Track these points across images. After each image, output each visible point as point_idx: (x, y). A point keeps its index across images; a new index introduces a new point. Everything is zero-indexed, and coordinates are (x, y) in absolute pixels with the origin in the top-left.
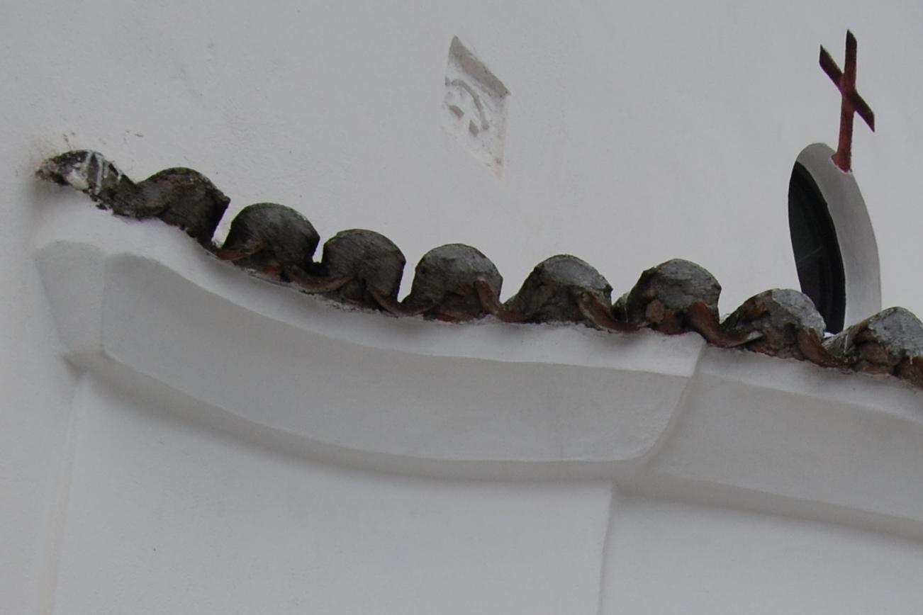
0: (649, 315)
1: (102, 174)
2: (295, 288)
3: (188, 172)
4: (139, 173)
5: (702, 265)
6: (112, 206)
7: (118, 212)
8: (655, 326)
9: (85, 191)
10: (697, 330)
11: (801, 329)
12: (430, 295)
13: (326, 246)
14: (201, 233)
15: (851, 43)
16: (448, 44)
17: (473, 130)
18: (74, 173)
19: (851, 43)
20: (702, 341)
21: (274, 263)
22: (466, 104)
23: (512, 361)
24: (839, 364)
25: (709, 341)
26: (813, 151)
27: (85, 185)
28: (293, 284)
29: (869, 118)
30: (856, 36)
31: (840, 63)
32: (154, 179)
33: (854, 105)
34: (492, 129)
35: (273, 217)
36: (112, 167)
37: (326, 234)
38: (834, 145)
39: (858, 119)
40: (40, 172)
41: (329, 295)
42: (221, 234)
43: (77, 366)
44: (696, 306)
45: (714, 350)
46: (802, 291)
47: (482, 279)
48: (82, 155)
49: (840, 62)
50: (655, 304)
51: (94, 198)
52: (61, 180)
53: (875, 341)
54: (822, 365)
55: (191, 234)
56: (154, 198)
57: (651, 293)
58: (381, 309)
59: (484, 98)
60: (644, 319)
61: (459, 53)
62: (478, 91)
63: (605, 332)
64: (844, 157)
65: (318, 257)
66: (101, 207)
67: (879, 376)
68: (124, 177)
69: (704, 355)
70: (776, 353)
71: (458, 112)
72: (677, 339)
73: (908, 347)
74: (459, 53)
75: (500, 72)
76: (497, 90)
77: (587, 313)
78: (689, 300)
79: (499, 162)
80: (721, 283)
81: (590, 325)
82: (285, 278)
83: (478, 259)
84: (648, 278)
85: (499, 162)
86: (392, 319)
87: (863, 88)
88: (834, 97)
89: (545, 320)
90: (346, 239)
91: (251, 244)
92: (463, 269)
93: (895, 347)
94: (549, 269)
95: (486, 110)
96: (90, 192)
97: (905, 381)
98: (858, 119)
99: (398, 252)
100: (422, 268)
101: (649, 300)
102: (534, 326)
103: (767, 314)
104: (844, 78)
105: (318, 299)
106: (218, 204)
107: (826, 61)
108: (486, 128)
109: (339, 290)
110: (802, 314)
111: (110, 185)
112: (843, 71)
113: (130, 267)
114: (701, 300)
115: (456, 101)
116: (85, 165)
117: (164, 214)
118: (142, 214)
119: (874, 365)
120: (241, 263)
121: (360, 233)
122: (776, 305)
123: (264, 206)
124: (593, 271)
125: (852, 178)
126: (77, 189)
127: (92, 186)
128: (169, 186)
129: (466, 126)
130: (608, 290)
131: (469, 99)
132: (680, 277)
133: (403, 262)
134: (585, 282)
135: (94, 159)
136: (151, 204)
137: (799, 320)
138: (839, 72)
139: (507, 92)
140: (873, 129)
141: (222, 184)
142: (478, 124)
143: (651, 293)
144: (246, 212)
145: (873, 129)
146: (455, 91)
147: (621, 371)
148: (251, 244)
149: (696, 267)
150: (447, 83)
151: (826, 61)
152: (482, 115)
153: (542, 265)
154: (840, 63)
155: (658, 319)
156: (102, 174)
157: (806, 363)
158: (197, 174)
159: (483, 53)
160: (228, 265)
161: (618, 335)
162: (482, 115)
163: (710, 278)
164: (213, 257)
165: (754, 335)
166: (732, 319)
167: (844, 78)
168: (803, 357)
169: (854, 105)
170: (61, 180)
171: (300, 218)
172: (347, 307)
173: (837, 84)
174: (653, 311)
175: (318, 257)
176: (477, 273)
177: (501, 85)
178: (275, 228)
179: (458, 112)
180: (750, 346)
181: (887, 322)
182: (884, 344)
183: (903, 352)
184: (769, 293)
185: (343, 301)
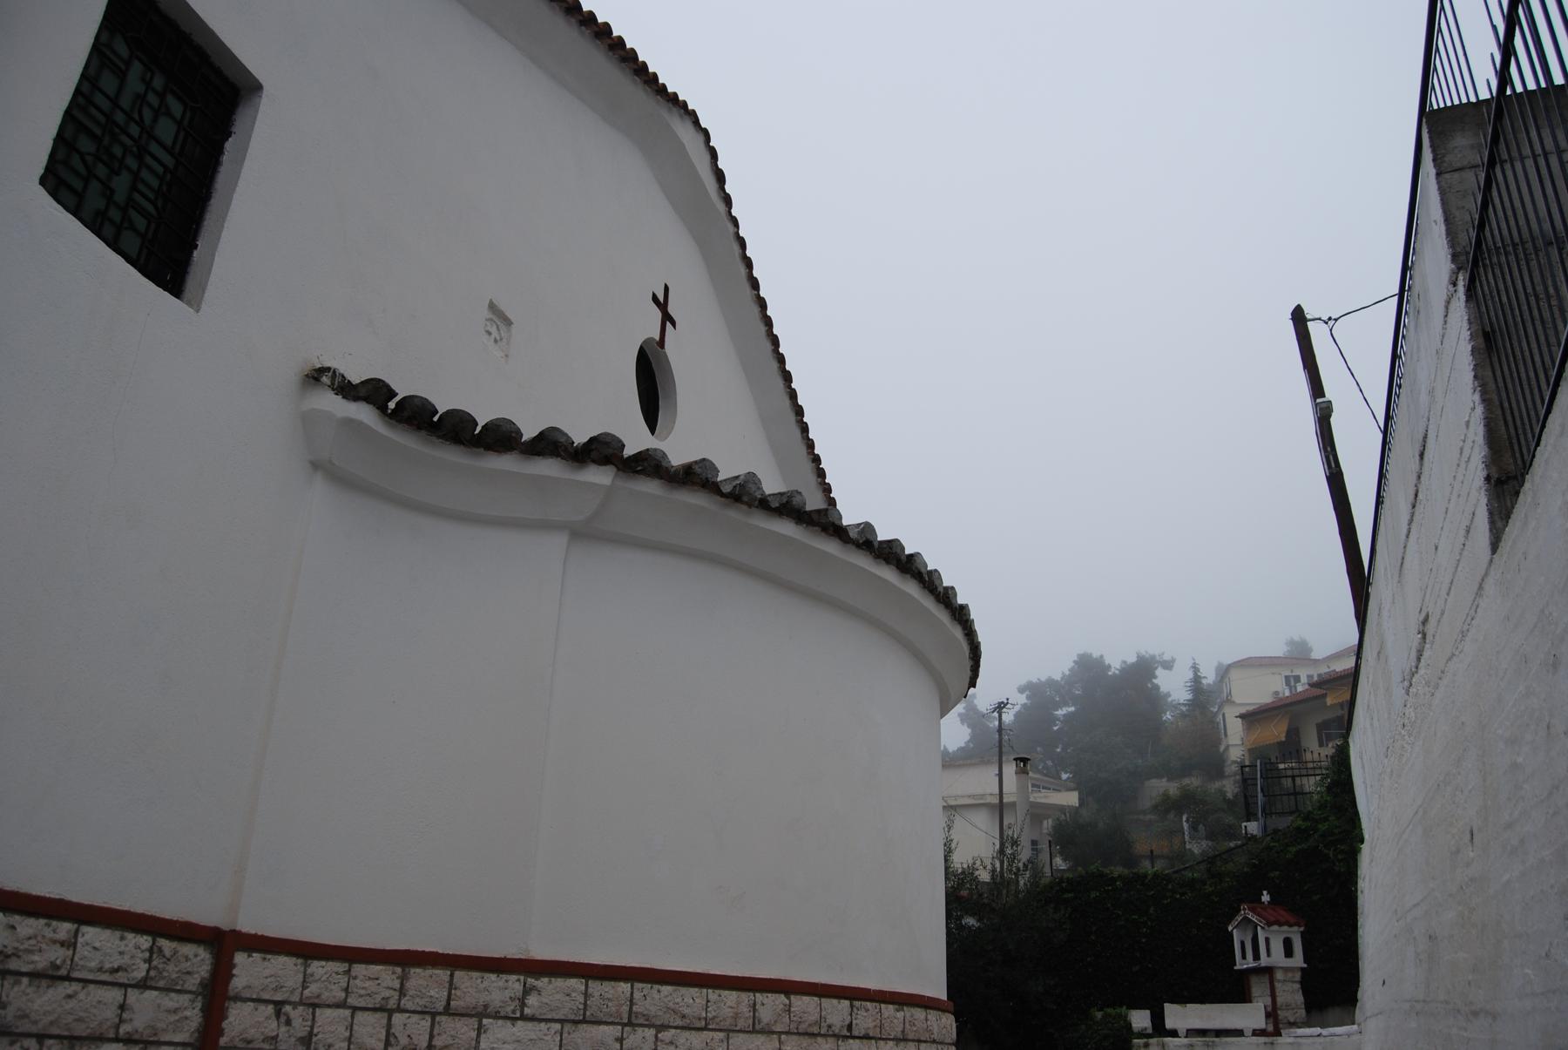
2: (423, 433)
4: (356, 380)
6: (342, 394)
7: (344, 397)
8: (594, 461)
9: (329, 386)
10: (613, 464)
11: (661, 466)
14: (382, 408)
15: (666, 289)
17: (496, 341)
18: (324, 377)
19: (666, 289)
20: (615, 469)
22: (493, 330)
23: (528, 472)
25: (619, 469)
26: (648, 341)
27: (329, 383)
28: (423, 431)
29: (674, 324)
31: (661, 300)
32: (362, 383)
33: (667, 318)
34: (504, 340)
36: (343, 376)
37: (442, 409)
38: (657, 338)
39: (668, 324)
40: (307, 376)
41: (439, 437)
43: (316, 466)
45: (620, 473)
47: (513, 435)
48: (329, 369)
51: (333, 389)
52: (317, 379)
53: (694, 473)
54: (670, 482)
55: (378, 408)
56: (363, 392)
57: (593, 447)
58: (464, 444)
59: (502, 327)
61: (492, 307)
62: (499, 323)
63: (570, 462)
64: (661, 343)
66: (337, 394)
68: (349, 381)
69: (616, 476)
70: (649, 476)
71: (489, 333)
73: (710, 476)
74: (492, 307)
76: (508, 322)
77: (562, 453)
78: (611, 451)
79: (507, 356)
80: (625, 443)
82: (419, 428)
83: (512, 425)
84: (592, 440)
85: (507, 356)
86: (469, 450)
87: (671, 310)
88: (658, 314)
90: (451, 413)
91: (406, 414)
92: (504, 429)
95: (502, 332)
96: (332, 387)
98: (668, 324)
99: (475, 420)
102: (537, 457)
103: (646, 459)
104: (662, 305)
105: (434, 438)
106: (393, 394)
107: (655, 298)
108: (501, 339)
109: (445, 435)
113: (349, 423)
114: (616, 451)
115: (489, 328)
116: (330, 374)
117: (367, 399)
118: (356, 399)
119: (693, 484)
120: (400, 421)
122: (650, 455)
123: (413, 396)
124: (566, 435)
126: (326, 385)
127: (333, 384)
131: (495, 326)
132: (607, 440)
133: (477, 425)
134: (563, 440)
135: (334, 372)
136: (361, 395)
137: (660, 462)
139: (512, 323)
140: (675, 328)
142: (498, 338)
143: (593, 447)
144: (404, 398)
145: (675, 328)
148: (406, 414)
149: (614, 436)
150: (486, 320)
152: (500, 334)
154: (661, 300)
159: (502, 306)
160: (393, 422)
162: (500, 334)
163: (620, 441)
164: (386, 418)
165: (639, 468)
167: (662, 305)
168: (661, 478)
169: (667, 318)
171: (430, 403)
172: (448, 443)
173: (658, 307)
174: (594, 455)
175: (436, 419)
176: (512, 432)
177: (509, 320)
179: (489, 333)
181: (700, 465)
182: (699, 475)
183: (707, 478)
184: (648, 450)
185: (446, 440)
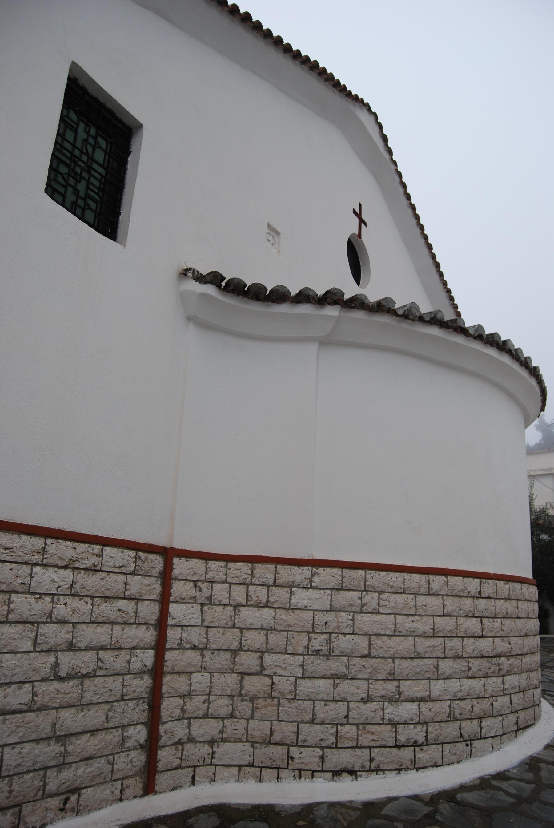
0: (327, 301)
1: (196, 274)
2: (240, 297)
3: (216, 272)
4: (204, 273)
5: (340, 289)
8: (329, 304)
10: (339, 304)
12: (274, 298)
13: (248, 287)
14: (219, 286)
15: (360, 205)
16: (267, 225)
17: (273, 244)
19: (360, 205)
21: (236, 292)
22: (271, 238)
24: (374, 311)
25: (342, 307)
26: (352, 235)
27: (192, 276)
29: (365, 224)
30: (361, 203)
32: (208, 274)
33: (362, 222)
34: (277, 243)
35: (236, 281)
36: (198, 272)
38: (357, 233)
39: (363, 225)
40: (180, 273)
41: (249, 298)
42: (223, 284)
44: (339, 299)
46: (533, 578)
48: (191, 269)
49: (358, 211)
50: (329, 298)
52: (185, 275)
53: (383, 306)
55: (217, 286)
56: (208, 279)
57: (328, 296)
58: (261, 301)
59: (275, 237)
60: (326, 302)
61: (269, 226)
64: (360, 235)
65: (246, 289)
66: (196, 281)
67: (384, 313)
69: (341, 310)
70: (358, 309)
71: (269, 241)
72: (334, 307)
74: (269, 226)
75: (278, 229)
76: (278, 233)
77: (312, 301)
78: (337, 297)
79: (279, 252)
81: (313, 303)
82: (238, 295)
84: (327, 292)
85: (279, 252)
87: (363, 217)
88: (357, 220)
89: (302, 303)
90: (253, 285)
91: (231, 288)
93: (388, 306)
94: (303, 291)
95: (275, 239)
97: (390, 314)
98: (363, 225)
100: (270, 291)
101: (327, 298)
103: (356, 300)
104: (358, 214)
105: (246, 299)
106: (223, 278)
107: (354, 211)
108: (275, 243)
110: (365, 300)
111: (198, 276)
112: (358, 213)
113: (204, 296)
115: (269, 238)
116: (192, 271)
117: (211, 282)
118: (205, 283)
119: (382, 311)
120: (228, 292)
121: (257, 284)
122: (358, 298)
125: (362, 241)
127: (193, 276)
128: (212, 276)
129: (271, 244)
130: (317, 295)
131: (271, 237)
133: (267, 290)
134: (312, 294)
135: (194, 270)
138: (357, 213)
141: (224, 274)
142: (274, 243)
143: (328, 296)
144: (229, 280)
146: (268, 235)
147: (321, 315)
148: (231, 288)
150: (267, 234)
151: (354, 211)
152: (274, 240)
153: (301, 290)
155: (330, 302)
156: (196, 274)
157: (366, 311)
158: (218, 272)
159: (275, 226)
160: (225, 293)
161: (319, 306)
162: (274, 240)
163: (342, 292)
164: (222, 291)
166: (347, 300)
167: (358, 214)
168: (365, 310)
169: (362, 222)
170: (185, 275)
171: (242, 281)
174: (328, 300)
175: (246, 289)
176: (285, 292)
178: (236, 283)
179: (269, 241)
180: (352, 307)
181: (385, 301)
182: (385, 306)
183: (389, 308)
184: (357, 295)
185: (252, 300)
